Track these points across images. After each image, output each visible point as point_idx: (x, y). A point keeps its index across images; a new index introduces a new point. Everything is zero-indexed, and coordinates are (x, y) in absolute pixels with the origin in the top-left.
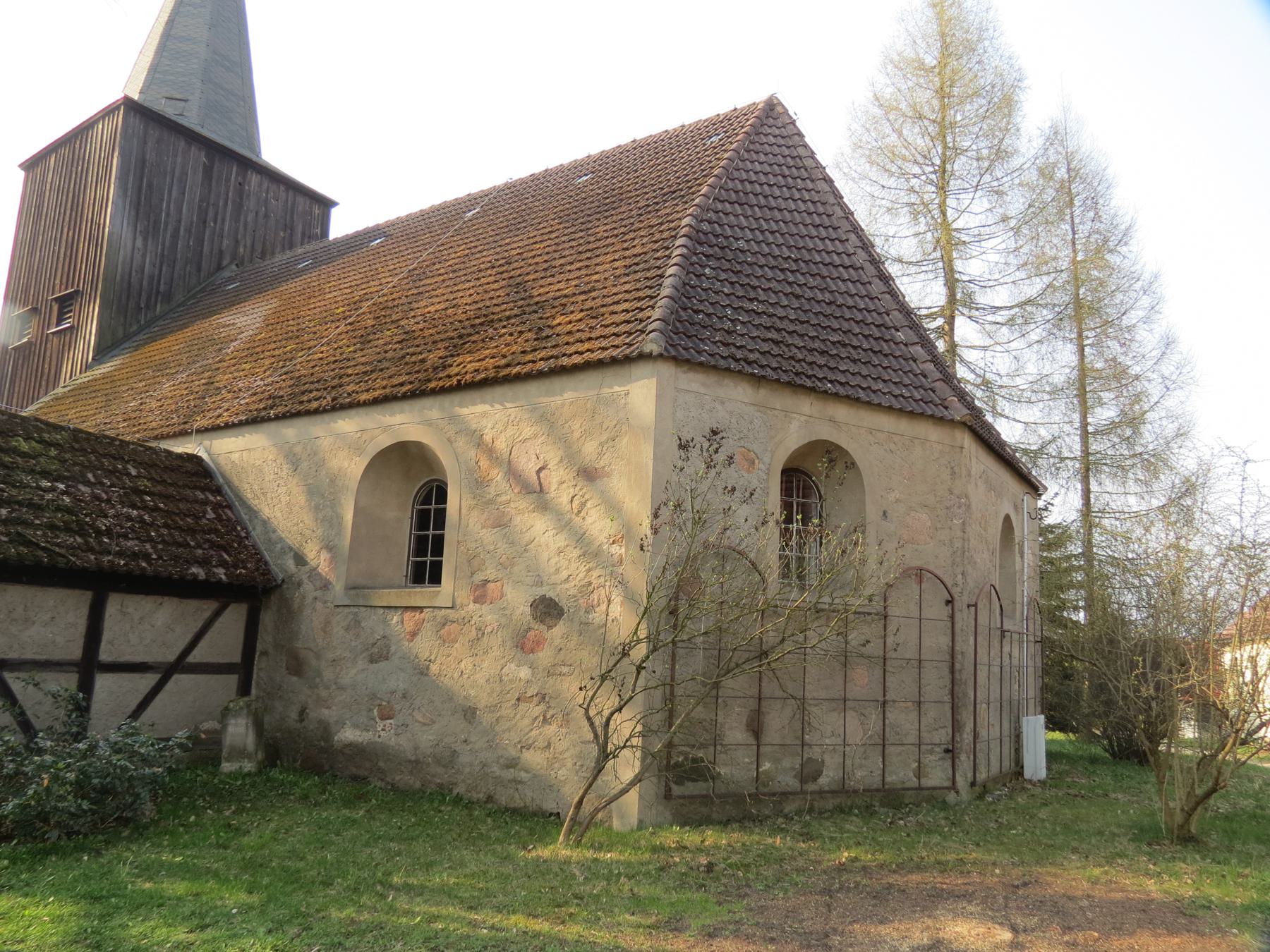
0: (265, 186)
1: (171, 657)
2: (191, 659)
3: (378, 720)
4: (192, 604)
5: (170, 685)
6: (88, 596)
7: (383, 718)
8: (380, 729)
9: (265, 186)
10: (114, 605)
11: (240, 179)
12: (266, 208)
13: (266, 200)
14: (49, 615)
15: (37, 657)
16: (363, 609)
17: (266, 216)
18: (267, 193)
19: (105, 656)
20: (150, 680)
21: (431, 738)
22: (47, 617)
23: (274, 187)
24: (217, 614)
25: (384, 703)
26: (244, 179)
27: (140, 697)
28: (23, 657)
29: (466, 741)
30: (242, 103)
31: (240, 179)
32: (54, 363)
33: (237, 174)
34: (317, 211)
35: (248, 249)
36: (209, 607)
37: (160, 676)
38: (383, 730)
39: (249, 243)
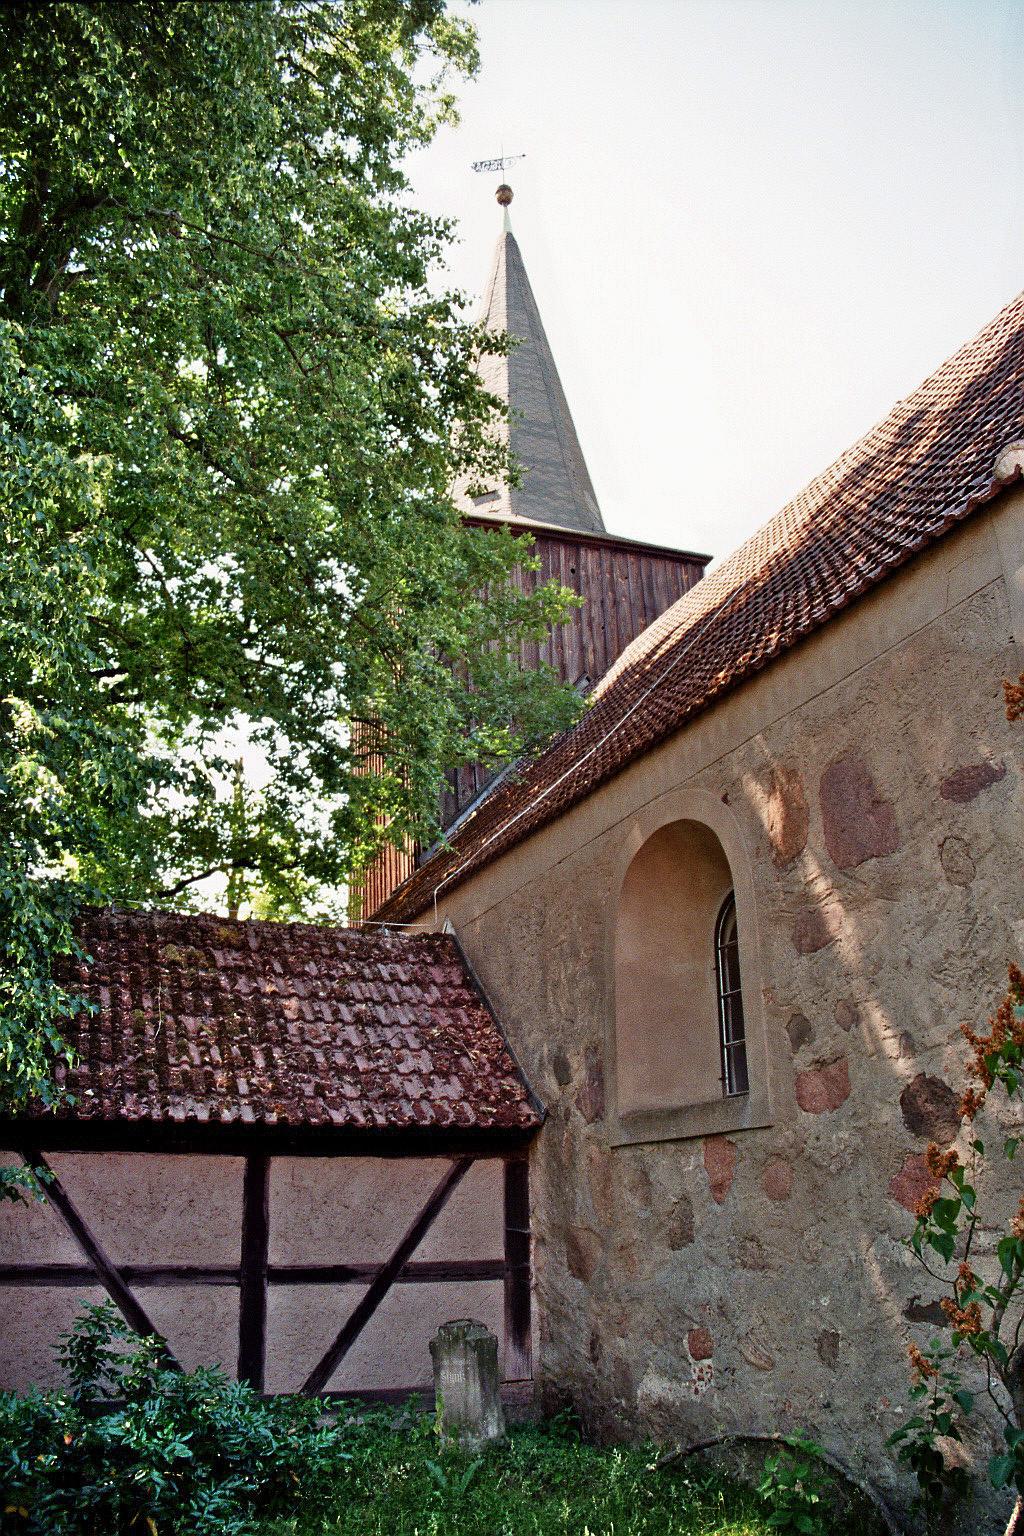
0: (606, 565)
1: (384, 1256)
2: (417, 1257)
3: (691, 1360)
4: (409, 1166)
5: (386, 1301)
6: (241, 1161)
7: (698, 1358)
8: (695, 1377)
9: (606, 565)
10: (281, 1170)
11: (572, 565)
12: (614, 592)
13: (612, 583)
14: (185, 1197)
15: (176, 1263)
16: (647, 1149)
17: (616, 603)
18: (611, 573)
19: (276, 1256)
20: (353, 1294)
21: (771, 1396)
22: (181, 1201)
23: (619, 560)
24: (453, 1179)
25: (696, 1327)
26: (577, 563)
27: (340, 1325)
28: (298, 1263)
29: (828, 1406)
30: (563, 471)
31: (572, 565)
32: (393, 863)
33: (567, 561)
34: (685, 577)
35: (600, 655)
36: (436, 1169)
37: (369, 1287)
38: (700, 1379)
39: (599, 645)
